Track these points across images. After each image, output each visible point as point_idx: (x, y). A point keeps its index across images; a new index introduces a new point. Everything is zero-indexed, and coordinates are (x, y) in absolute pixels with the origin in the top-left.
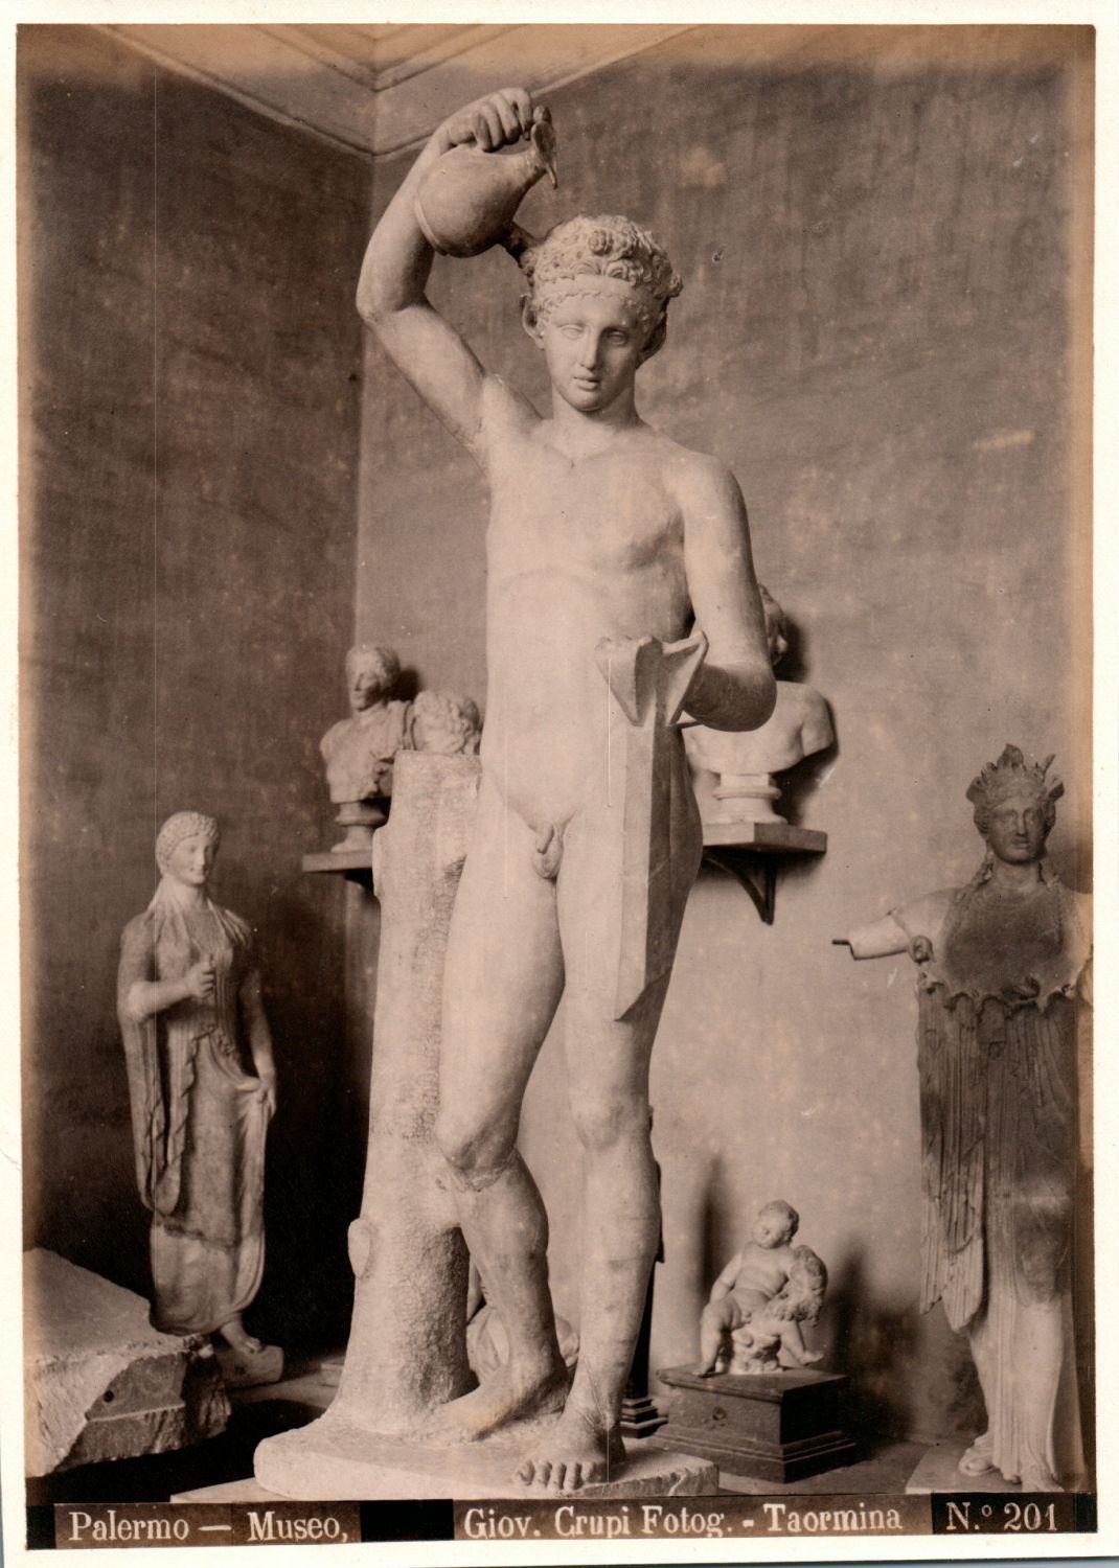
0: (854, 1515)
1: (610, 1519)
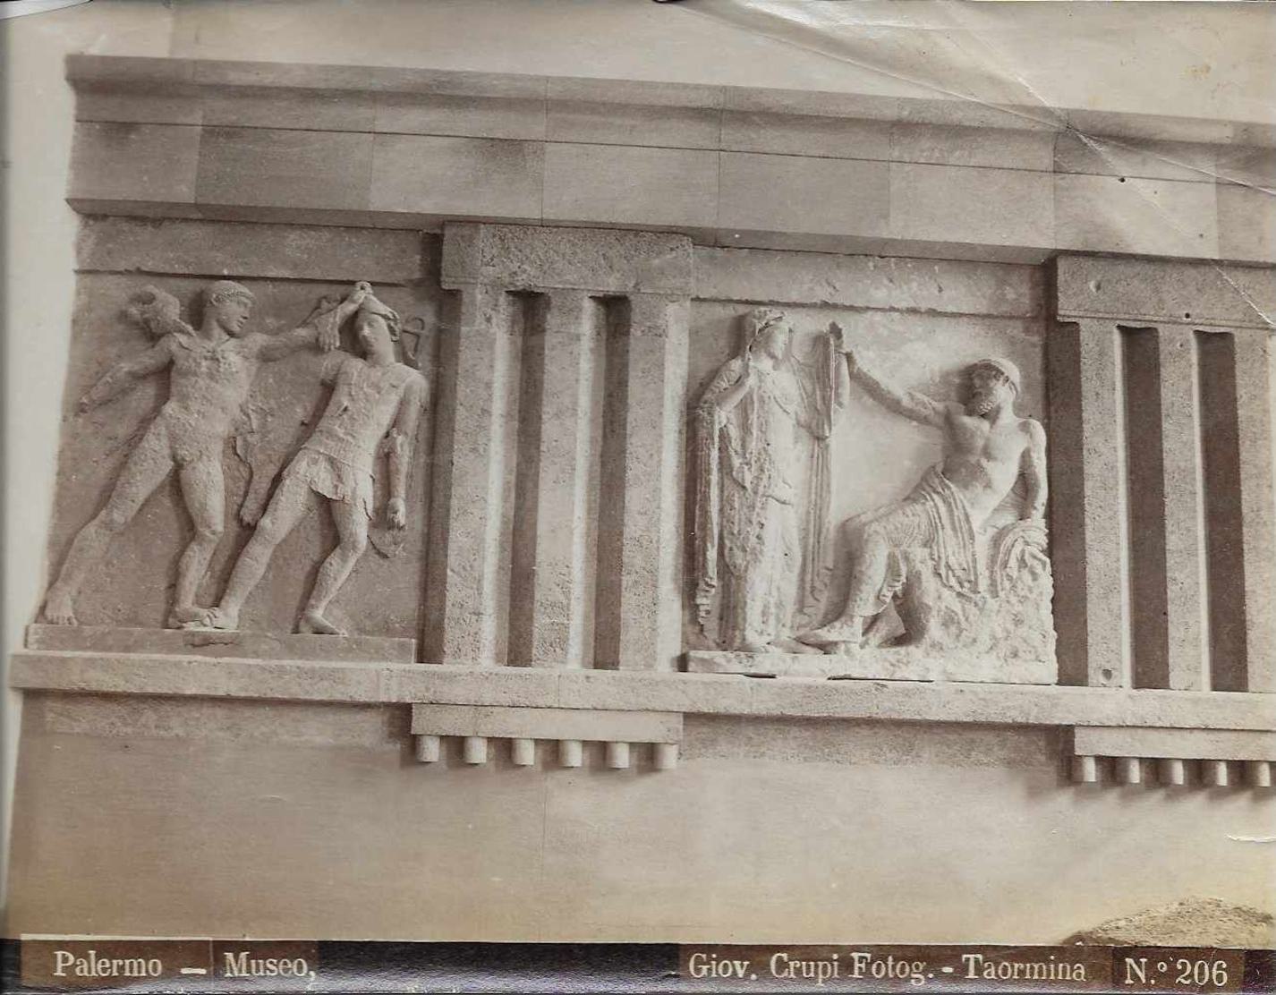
0: (829, 967)
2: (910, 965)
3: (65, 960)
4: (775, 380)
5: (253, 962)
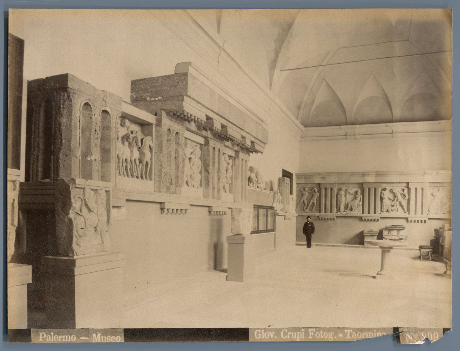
0: (301, 334)
1: (298, 333)
3: (43, 335)
4: (343, 193)
5: (102, 337)
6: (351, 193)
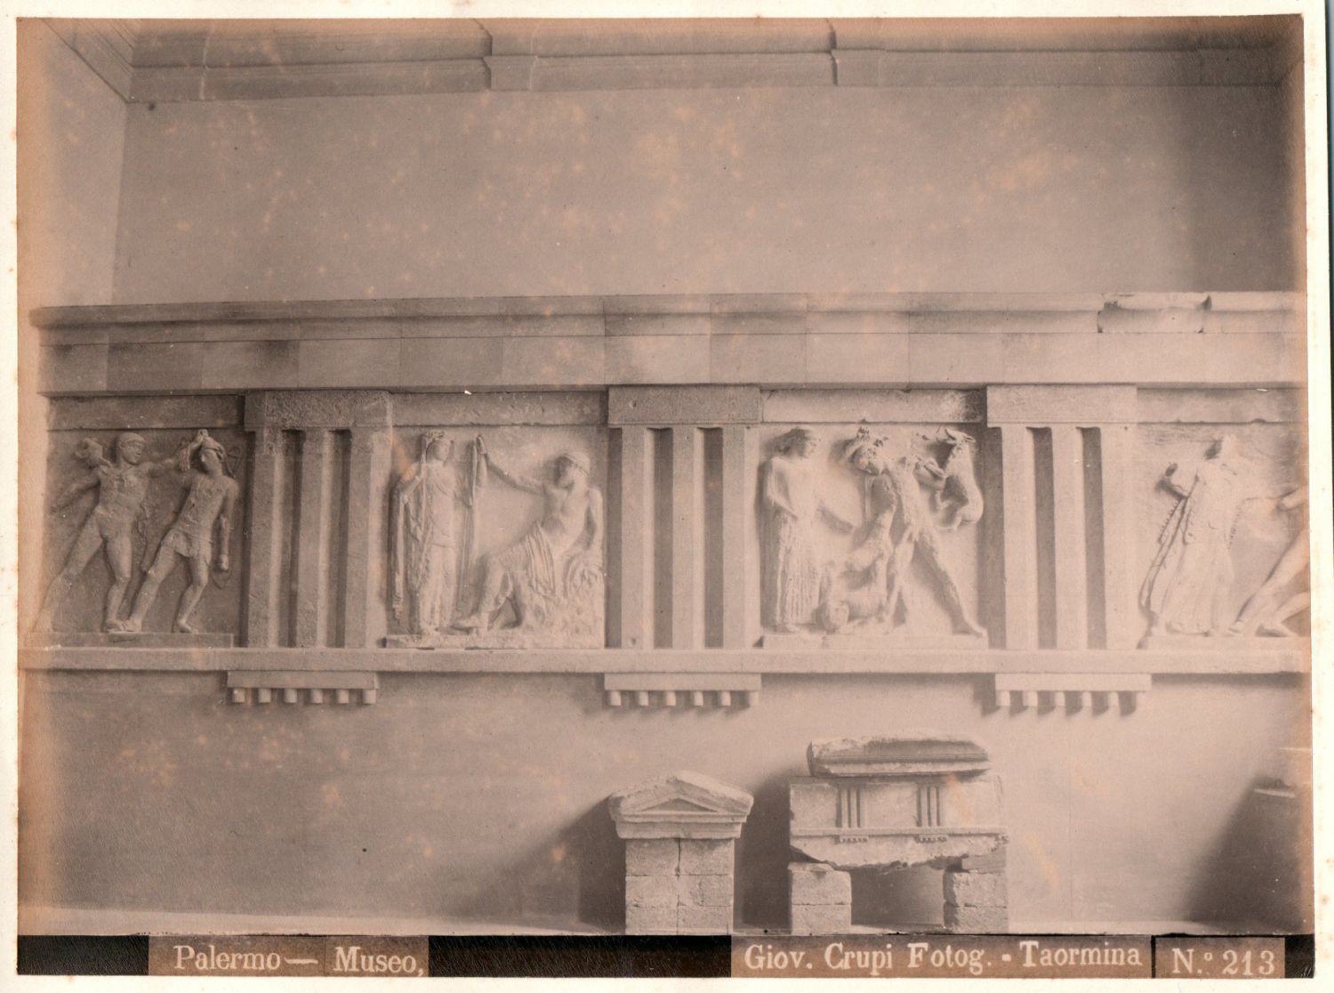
0: (883, 957)
1: (875, 954)
2: (968, 954)
3: (185, 952)
6: (516, 476)
